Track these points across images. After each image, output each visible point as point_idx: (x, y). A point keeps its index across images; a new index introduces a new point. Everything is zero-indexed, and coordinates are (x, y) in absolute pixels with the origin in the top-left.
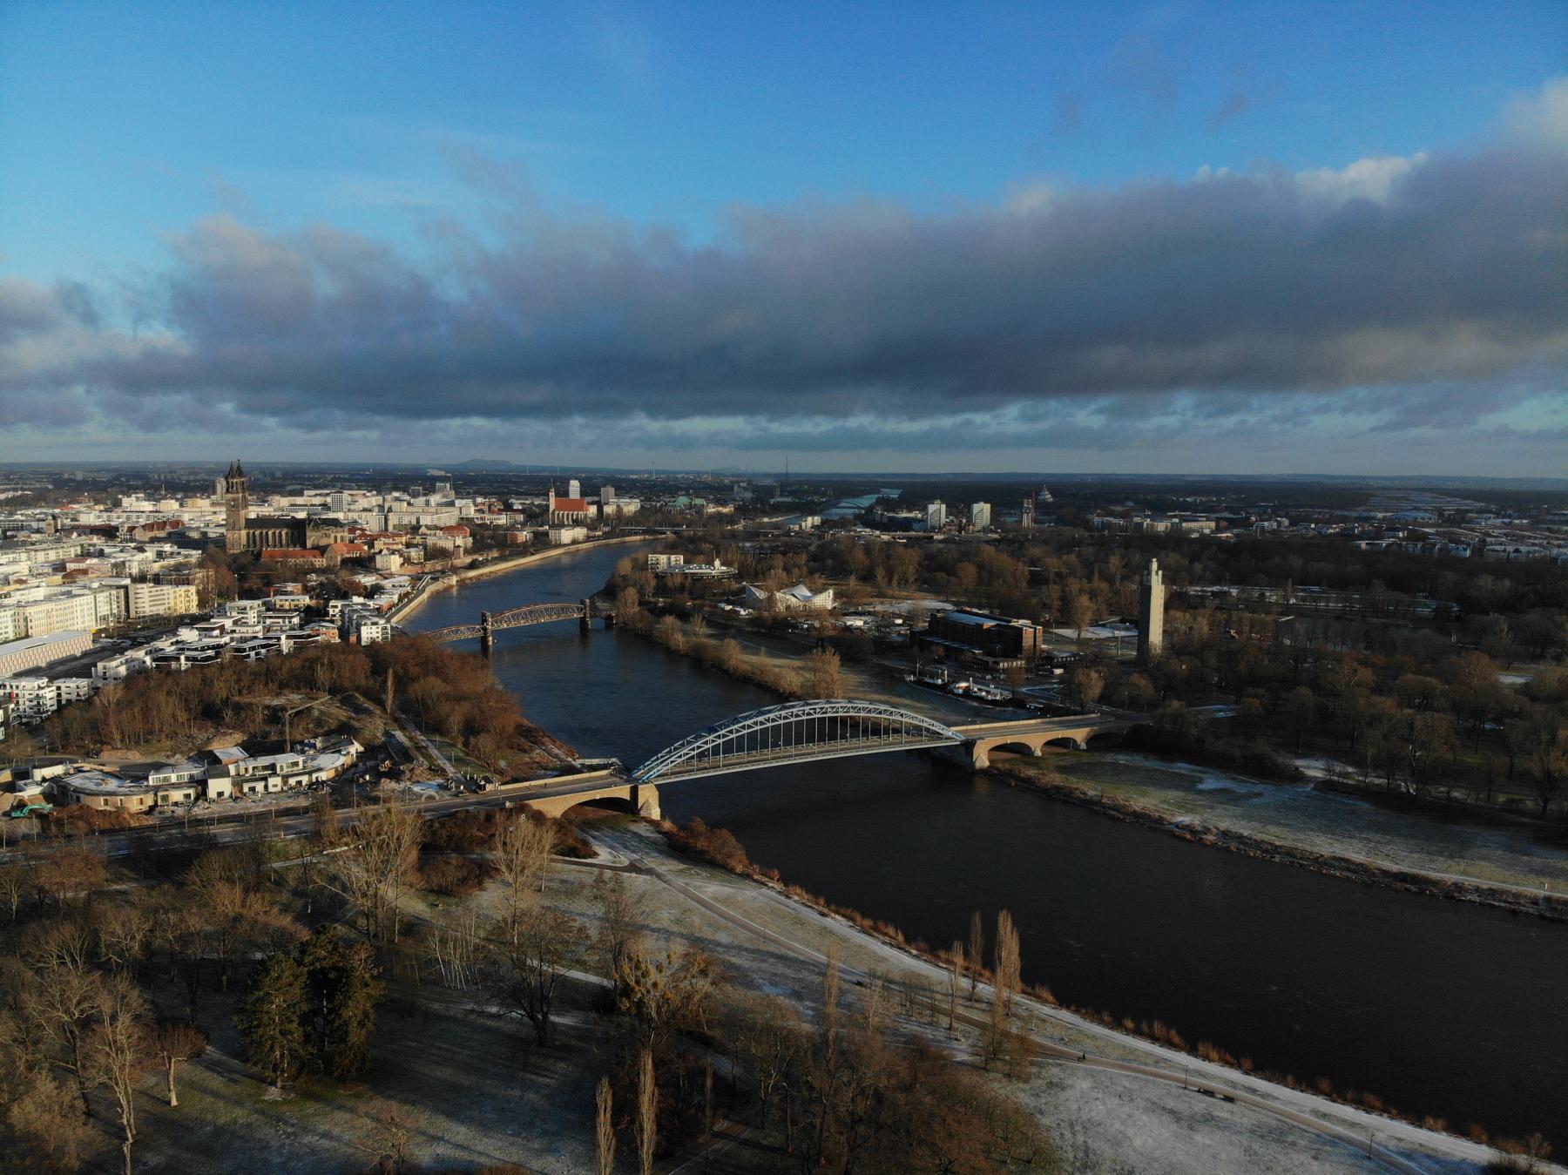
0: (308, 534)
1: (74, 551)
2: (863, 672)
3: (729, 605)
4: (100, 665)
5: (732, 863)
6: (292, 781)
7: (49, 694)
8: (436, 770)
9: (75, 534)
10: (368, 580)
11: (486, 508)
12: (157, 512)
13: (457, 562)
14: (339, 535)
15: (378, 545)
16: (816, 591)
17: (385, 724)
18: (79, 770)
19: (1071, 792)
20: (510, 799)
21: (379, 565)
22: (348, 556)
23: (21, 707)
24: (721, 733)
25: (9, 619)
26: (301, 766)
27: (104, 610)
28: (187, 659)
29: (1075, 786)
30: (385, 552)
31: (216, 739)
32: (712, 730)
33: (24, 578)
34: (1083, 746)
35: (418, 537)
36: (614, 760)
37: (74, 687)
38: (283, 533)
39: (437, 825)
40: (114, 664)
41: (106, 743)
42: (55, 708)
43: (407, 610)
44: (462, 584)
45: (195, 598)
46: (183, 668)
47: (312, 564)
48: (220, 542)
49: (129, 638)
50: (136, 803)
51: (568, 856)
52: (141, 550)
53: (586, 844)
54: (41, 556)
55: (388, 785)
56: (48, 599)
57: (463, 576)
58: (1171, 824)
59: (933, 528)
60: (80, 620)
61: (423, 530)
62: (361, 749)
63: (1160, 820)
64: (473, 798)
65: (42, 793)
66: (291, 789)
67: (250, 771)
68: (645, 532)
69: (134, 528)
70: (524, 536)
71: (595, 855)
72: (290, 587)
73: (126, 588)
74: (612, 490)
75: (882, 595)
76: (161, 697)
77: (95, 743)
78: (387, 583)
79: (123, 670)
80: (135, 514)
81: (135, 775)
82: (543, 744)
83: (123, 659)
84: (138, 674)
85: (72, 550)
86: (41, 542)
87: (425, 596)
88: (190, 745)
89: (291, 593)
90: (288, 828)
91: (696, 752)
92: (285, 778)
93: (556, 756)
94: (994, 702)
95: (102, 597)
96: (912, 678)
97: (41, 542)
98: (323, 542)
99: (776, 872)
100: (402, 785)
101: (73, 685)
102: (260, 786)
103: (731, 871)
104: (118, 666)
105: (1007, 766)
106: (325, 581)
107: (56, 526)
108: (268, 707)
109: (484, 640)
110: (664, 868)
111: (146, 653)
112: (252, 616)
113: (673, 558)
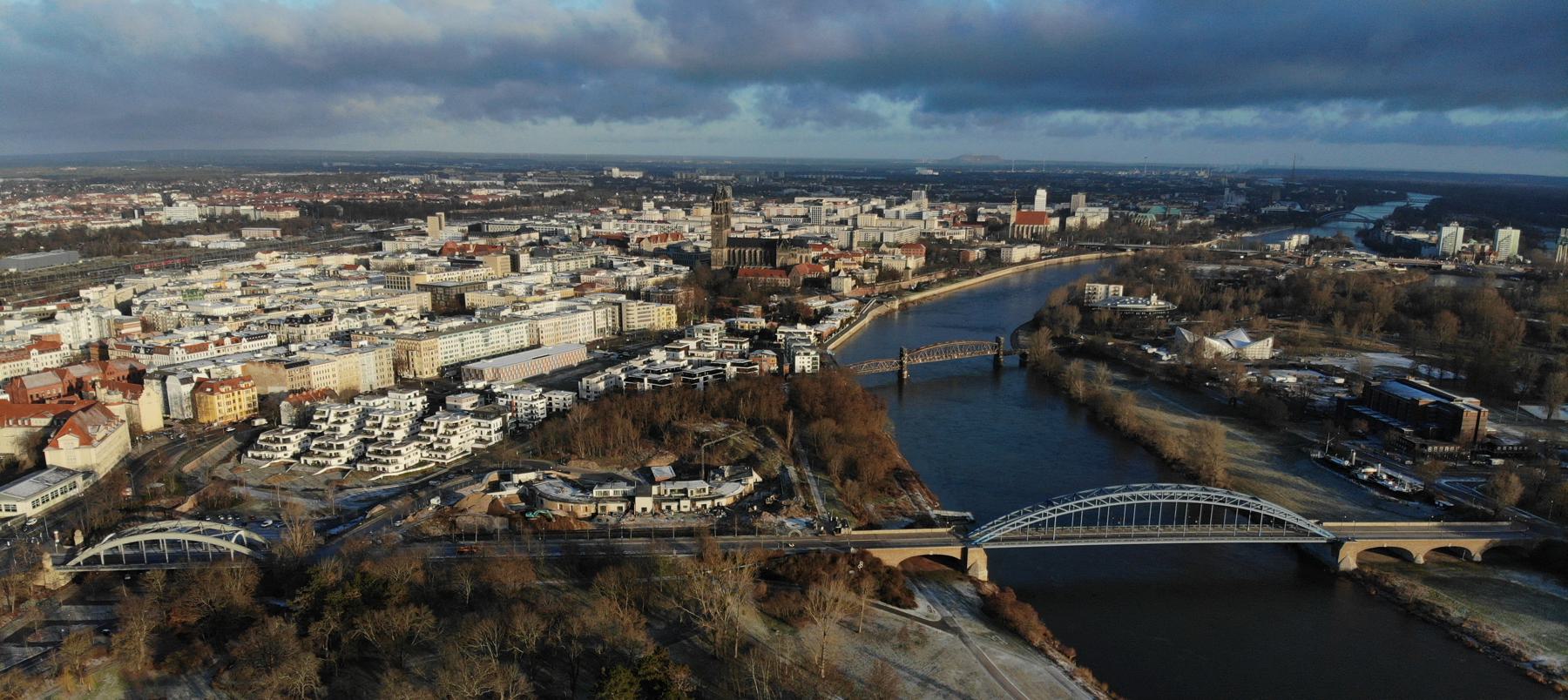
0: (778, 254)
1: (590, 262)
2: (1268, 441)
3: (1153, 347)
4: (584, 380)
5: (1032, 634)
6: (699, 504)
7: (541, 405)
8: (809, 508)
9: (594, 244)
10: (817, 303)
11: (950, 221)
12: (665, 222)
13: (904, 285)
14: (804, 256)
15: (839, 265)
16: (1256, 338)
17: (783, 459)
18: (548, 477)
19: (1432, 611)
20: (856, 545)
21: (833, 287)
22: (809, 276)
23: (519, 414)
24: (1056, 508)
25: (524, 330)
26: (707, 492)
27: (601, 324)
28: (649, 381)
29: (1440, 604)
30: (842, 274)
31: (655, 458)
32: (1049, 504)
33: (544, 289)
34: (1478, 557)
35: (875, 256)
36: (968, 514)
37: (561, 398)
38: (758, 252)
39: (791, 561)
40: (595, 380)
41: (575, 454)
42: (545, 416)
43: (846, 335)
44: (904, 307)
45: (674, 316)
46: (646, 388)
47: (777, 284)
48: (706, 258)
49: (617, 351)
50: (583, 510)
51: (891, 604)
52: (641, 264)
53: (911, 594)
54: (563, 266)
55: (768, 517)
56: (557, 313)
57: (906, 299)
58: (1528, 661)
59: (1445, 255)
60: (581, 332)
61: (883, 247)
62: (760, 479)
63: (1518, 656)
64: (829, 539)
65: (518, 493)
66: (698, 510)
67: (669, 493)
68: (1104, 249)
69: (642, 239)
70: (976, 254)
71: (915, 606)
72: (752, 309)
73: (620, 304)
74: (1081, 197)
75: (1337, 344)
76: (618, 419)
77: (566, 451)
78: (836, 306)
79: (602, 386)
80: (646, 224)
81: (584, 485)
82: (911, 490)
83: (603, 376)
84: (614, 390)
85: (589, 260)
86: (566, 251)
87: (867, 320)
88: (636, 461)
89: (752, 315)
90: (681, 548)
91: (1029, 523)
92: (694, 501)
93: (918, 504)
94: (1399, 494)
95: (600, 313)
96: (1319, 455)
97: (566, 251)
98: (791, 261)
99: (1073, 651)
100: (780, 519)
101: (561, 397)
102: (674, 506)
103: (1028, 643)
104: (598, 382)
105: (1375, 572)
106: (785, 302)
107: (580, 235)
108: (697, 434)
109: (900, 373)
110: (969, 629)
111: (622, 371)
112: (714, 339)
113: (1112, 288)
